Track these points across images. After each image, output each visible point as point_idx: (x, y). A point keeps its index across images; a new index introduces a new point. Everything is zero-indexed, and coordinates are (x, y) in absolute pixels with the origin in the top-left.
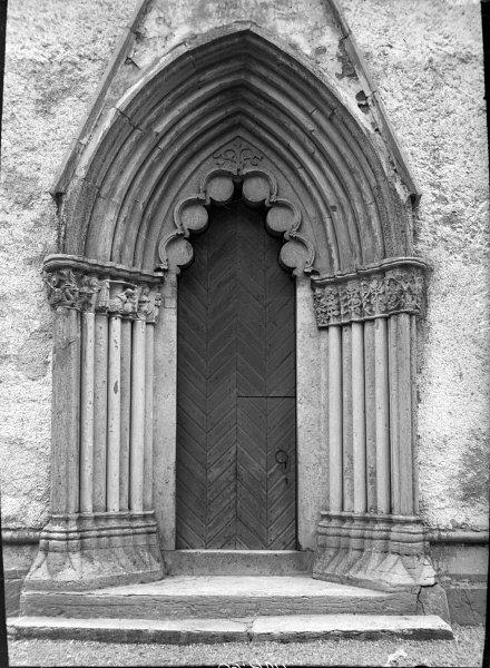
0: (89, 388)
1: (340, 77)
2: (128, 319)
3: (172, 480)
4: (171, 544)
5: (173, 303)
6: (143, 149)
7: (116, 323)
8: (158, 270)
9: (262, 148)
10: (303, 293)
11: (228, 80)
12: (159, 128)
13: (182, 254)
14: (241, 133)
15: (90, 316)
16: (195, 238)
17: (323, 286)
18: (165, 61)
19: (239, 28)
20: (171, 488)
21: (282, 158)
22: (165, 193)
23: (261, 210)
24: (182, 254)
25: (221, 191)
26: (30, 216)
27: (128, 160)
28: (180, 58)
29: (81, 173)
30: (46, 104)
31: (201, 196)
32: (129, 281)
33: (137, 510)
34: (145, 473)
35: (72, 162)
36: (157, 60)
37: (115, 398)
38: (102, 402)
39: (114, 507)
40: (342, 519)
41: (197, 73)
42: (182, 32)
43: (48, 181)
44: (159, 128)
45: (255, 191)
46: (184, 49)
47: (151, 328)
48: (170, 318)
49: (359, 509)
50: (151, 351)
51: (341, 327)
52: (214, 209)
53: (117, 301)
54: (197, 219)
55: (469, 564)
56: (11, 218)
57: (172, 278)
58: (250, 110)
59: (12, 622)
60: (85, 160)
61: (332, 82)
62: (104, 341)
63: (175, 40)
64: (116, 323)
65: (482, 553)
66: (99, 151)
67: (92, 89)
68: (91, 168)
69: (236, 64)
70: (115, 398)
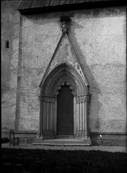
0: (44, 112)
1: (78, 69)
2: (50, 103)
3: (56, 125)
4: (56, 134)
5: (56, 100)
6: (52, 79)
7: (48, 103)
8: (54, 95)
9: (69, 78)
10: (75, 98)
11: (63, 69)
12: (54, 76)
13: (57, 93)
14: (66, 76)
15: (44, 103)
16: (59, 91)
17: (77, 97)
18: (54, 68)
19: (64, 63)
20: (56, 127)
21: (71, 79)
22: (55, 85)
23: (69, 86)
24: (57, 93)
25: (63, 84)
26: (37, 89)
27: (50, 80)
28: (56, 67)
29: (43, 83)
30: (39, 74)
31: (60, 85)
32: (50, 97)
33: (51, 129)
34: (52, 124)
35: (42, 82)
36: (53, 68)
37: (48, 114)
38: (46, 114)
39: (48, 129)
40: (79, 131)
41: (59, 69)
42: (56, 64)
43: (39, 84)
44: (54, 76)
45: (68, 84)
46: (56, 66)
47: (53, 104)
48: (56, 102)
49: (81, 129)
50: (53, 106)
51: (82, 103)
52: (62, 86)
53: (48, 100)
54: (60, 88)
55: (124, 138)
56: (34, 89)
57: (56, 96)
58: (66, 74)
59: (2, 131)
60: (43, 82)
61: (77, 70)
62: (46, 106)
63: (55, 65)
64: (48, 103)
65: (125, 136)
66: (45, 81)
67: (45, 72)
68: (44, 83)
69: (64, 67)
70: (48, 114)
